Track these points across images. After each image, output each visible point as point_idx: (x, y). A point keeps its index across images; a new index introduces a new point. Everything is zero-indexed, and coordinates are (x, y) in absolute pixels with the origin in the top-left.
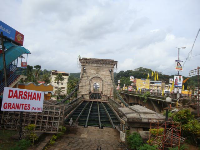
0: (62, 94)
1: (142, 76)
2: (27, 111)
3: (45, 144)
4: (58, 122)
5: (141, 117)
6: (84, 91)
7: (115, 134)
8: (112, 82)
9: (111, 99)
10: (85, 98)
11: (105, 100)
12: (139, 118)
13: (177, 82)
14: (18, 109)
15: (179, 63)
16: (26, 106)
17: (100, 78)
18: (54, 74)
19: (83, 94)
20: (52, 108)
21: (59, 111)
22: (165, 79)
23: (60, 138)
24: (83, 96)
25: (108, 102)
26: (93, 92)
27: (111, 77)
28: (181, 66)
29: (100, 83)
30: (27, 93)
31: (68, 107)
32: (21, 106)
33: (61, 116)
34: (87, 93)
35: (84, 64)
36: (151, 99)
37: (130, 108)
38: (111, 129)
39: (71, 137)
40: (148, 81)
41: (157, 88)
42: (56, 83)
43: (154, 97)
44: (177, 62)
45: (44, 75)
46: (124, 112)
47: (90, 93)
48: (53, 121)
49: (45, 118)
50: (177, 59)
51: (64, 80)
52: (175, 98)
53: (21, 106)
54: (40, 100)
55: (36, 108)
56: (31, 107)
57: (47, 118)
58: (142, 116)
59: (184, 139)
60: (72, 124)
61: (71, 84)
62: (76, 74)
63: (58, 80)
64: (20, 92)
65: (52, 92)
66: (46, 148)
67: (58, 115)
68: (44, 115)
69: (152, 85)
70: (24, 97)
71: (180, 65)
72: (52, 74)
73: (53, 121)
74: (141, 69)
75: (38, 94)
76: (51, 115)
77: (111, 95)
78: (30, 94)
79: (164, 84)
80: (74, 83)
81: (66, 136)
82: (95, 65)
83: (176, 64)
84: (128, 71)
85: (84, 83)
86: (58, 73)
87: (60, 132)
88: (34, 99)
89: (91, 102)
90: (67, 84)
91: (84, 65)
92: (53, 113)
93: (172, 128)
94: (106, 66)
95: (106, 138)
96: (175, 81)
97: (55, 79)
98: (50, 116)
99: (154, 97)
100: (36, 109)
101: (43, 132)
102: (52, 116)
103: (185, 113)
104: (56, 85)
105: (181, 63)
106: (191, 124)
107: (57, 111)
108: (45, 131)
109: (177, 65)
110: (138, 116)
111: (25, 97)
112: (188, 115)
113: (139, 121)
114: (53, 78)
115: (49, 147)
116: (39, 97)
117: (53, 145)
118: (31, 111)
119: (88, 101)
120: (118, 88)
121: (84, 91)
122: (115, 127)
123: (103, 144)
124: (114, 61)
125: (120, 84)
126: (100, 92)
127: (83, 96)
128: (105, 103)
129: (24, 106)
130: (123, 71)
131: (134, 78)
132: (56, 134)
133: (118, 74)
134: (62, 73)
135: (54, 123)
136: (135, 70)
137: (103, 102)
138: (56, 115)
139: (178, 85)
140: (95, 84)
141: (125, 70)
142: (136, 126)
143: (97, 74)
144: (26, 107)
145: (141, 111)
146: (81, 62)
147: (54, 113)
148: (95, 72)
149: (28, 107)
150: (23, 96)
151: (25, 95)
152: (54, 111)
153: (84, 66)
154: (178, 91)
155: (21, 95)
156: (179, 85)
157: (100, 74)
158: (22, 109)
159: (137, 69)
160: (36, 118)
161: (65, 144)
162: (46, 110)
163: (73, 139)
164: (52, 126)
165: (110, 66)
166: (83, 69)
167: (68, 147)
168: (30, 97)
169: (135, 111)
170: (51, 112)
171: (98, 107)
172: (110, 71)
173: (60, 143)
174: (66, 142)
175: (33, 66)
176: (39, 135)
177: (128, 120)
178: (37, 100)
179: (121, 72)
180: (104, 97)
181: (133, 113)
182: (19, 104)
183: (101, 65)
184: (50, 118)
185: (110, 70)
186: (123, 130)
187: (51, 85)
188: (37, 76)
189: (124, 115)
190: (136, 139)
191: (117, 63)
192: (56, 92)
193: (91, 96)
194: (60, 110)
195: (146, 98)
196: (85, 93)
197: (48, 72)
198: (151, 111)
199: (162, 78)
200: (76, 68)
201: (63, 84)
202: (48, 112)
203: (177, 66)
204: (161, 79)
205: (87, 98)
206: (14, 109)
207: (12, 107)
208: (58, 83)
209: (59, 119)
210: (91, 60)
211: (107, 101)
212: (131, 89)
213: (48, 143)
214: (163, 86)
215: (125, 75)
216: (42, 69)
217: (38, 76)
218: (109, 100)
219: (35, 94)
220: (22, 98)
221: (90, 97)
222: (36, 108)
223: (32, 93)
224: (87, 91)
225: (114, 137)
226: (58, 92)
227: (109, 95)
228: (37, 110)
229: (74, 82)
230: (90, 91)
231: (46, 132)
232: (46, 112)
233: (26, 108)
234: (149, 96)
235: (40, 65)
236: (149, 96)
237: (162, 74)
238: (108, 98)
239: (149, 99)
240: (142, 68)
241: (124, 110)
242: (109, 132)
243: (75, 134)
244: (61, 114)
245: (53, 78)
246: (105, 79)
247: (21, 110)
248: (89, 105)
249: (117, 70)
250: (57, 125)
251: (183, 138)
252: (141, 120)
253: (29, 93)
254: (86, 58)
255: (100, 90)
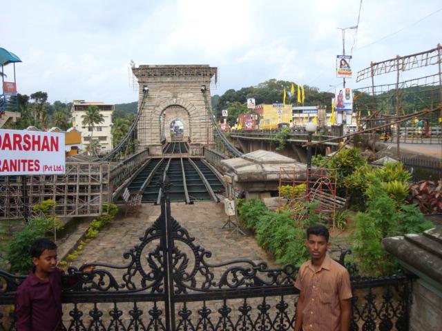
0: (103, 151)
1: (275, 97)
2: (34, 173)
3: (79, 237)
4: (100, 194)
5: (264, 171)
6: (150, 138)
7: (218, 212)
8: (209, 113)
9: (210, 149)
10: (153, 153)
11: (196, 155)
12: (261, 173)
13: (342, 101)
14: (15, 170)
15: (345, 61)
16: (31, 163)
17: (181, 107)
18: (78, 108)
19: (148, 144)
20: (84, 167)
21: (100, 173)
22: (321, 100)
23: (106, 226)
24: (148, 150)
25: (202, 157)
26: (169, 140)
27: (206, 102)
28: (348, 67)
29: (184, 119)
30: (29, 138)
31: (116, 167)
32: (22, 164)
33: (105, 182)
34: (156, 141)
35: (144, 80)
36: (292, 142)
37: (245, 158)
38: (208, 204)
39: (130, 223)
40: (288, 108)
41: (309, 121)
42: (87, 129)
43: (298, 137)
44: (339, 60)
45: (56, 114)
46: (233, 166)
47: (164, 142)
48: (89, 194)
49: (71, 188)
50: (341, 53)
51: (103, 120)
52: (339, 134)
53: (22, 164)
54: (57, 150)
55: (51, 167)
56: (41, 165)
57: (76, 188)
58: (268, 168)
59: (345, 200)
60: (130, 199)
61: (119, 128)
62: (129, 104)
63: (90, 121)
64: (15, 136)
65: (80, 147)
66: (82, 242)
67: (99, 179)
68: (70, 184)
69: (296, 115)
70: (24, 146)
71: (346, 65)
72: (73, 108)
73: (89, 194)
74: (272, 84)
75: (52, 138)
76: (84, 182)
77: (208, 142)
78: (36, 139)
79: (322, 111)
80: (126, 125)
81: (118, 222)
82: (169, 79)
83: (339, 64)
84: (243, 89)
85: (147, 122)
86: (87, 106)
87: (105, 214)
88: (45, 150)
89: (166, 160)
90: (110, 128)
91: (144, 82)
92: (87, 177)
93: (320, 181)
94: (193, 80)
95: (199, 218)
96: (338, 100)
97: (83, 119)
98: (82, 184)
99: (298, 137)
100: (53, 169)
101: (70, 216)
102: (86, 184)
103: (349, 155)
104: (86, 133)
105: (347, 60)
106: (359, 174)
107: (94, 173)
108: (75, 213)
109: (341, 65)
110: (260, 169)
111: (27, 146)
112: (354, 157)
113: (261, 177)
114: (78, 118)
115: (88, 242)
116: (55, 144)
117: (94, 238)
118: (43, 173)
119: (160, 159)
120: (224, 127)
121: (150, 138)
122: (218, 199)
123: (194, 228)
124: (210, 68)
125: (229, 120)
126: (185, 140)
127: (148, 150)
128: (196, 160)
129: (27, 164)
130: (234, 91)
131: (257, 104)
132: (97, 219)
133: (223, 96)
134: (98, 106)
135: (92, 197)
136: (260, 85)
137: (191, 159)
138: (93, 181)
139: (344, 107)
140: (174, 122)
141: (237, 88)
142: (257, 189)
143: (175, 100)
144: (32, 165)
145: (264, 159)
146: (137, 76)
147: (90, 178)
148: (170, 95)
149: (34, 166)
150: (23, 143)
151: (26, 142)
152: (89, 174)
153: (144, 84)
154: (344, 119)
155: (19, 143)
156: (346, 108)
157: (181, 98)
158: (24, 170)
159: (264, 83)
160: (55, 190)
161: (118, 234)
162: (73, 174)
163: (134, 225)
164: (88, 203)
165: (200, 79)
166: (144, 90)
167: (125, 238)
168: (36, 146)
169: (253, 161)
170: (84, 176)
171: (183, 169)
172: (202, 90)
173: (108, 234)
174: (120, 232)
175: (29, 95)
176: (66, 222)
177: (239, 178)
178: (52, 150)
179: (228, 92)
180: (195, 146)
181: (249, 165)
182: (16, 161)
183: (182, 79)
184: (82, 188)
185: (203, 88)
186: (230, 195)
187: (75, 130)
188: (41, 117)
189: (232, 170)
190: (254, 208)
191: (216, 72)
192: (88, 148)
193: (165, 149)
194: (101, 169)
195: (281, 141)
196: (153, 141)
197: (64, 105)
198: (285, 157)
199: (320, 100)
200: (129, 93)
201: (103, 129)
202: (76, 176)
203: (341, 67)
204: (318, 102)
205: (158, 152)
206: (8, 170)
207: (4, 168)
208: (90, 129)
209: (101, 188)
210: (158, 69)
211: (200, 155)
212: (250, 127)
213: (84, 235)
214: (322, 117)
215: (235, 99)
216: (51, 100)
217: (44, 116)
218: (206, 153)
219: (46, 138)
220: (20, 149)
221: (163, 151)
222: (51, 167)
223: (39, 137)
224: (155, 138)
225: (216, 215)
226: (92, 148)
227: (204, 143)
228: (55, 170)
229: (126, 123)
230: (163, 140)
231: (77, 215)
232: (72, 176)
233: (31, 167)
234: (289, 137)
235: (43, 91)
236: (289, 137)
237: (319, 92)
238: (204, 148)
239: (288, 142)
240: (274, 80)
241: (231, 162)
242: (205, 209)
243: (137, 217)
244: (104, 179)
245: (78, 118)
246: (193, 108)
247: (22, 173)
248: (163, 165)
249: (218, 89)
250: (98, 201)
251: (343, 199)
252: (266, 175)
253: (34, 136)
254: (148, 66)
255: (184, 135)
